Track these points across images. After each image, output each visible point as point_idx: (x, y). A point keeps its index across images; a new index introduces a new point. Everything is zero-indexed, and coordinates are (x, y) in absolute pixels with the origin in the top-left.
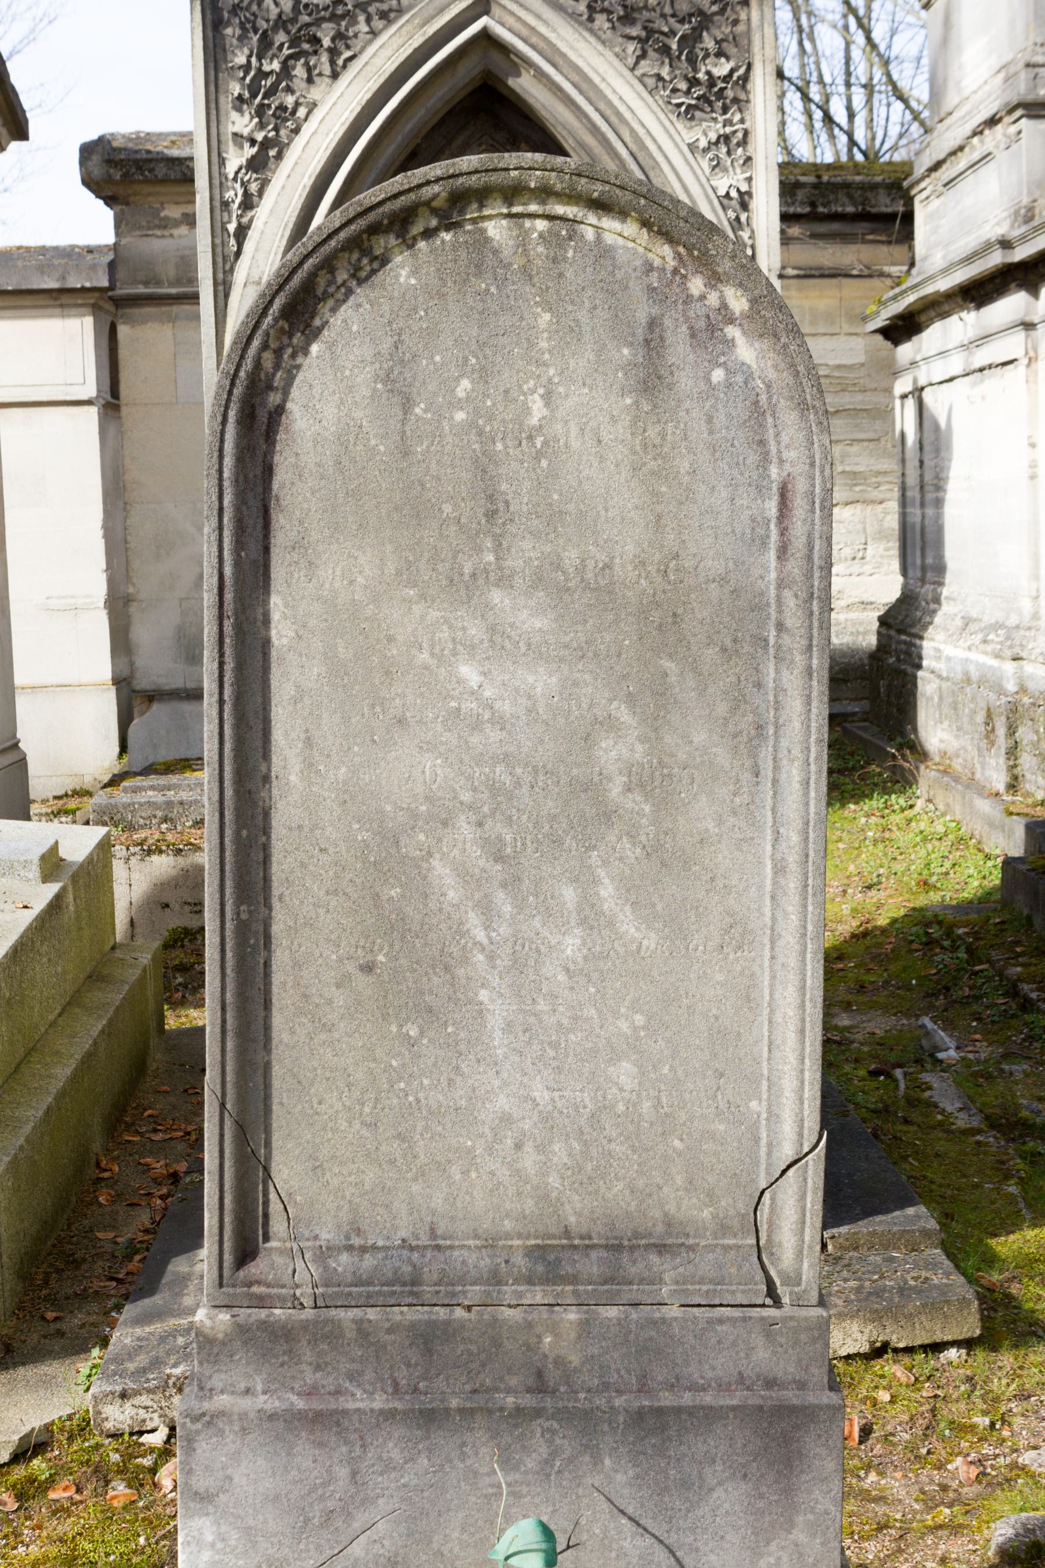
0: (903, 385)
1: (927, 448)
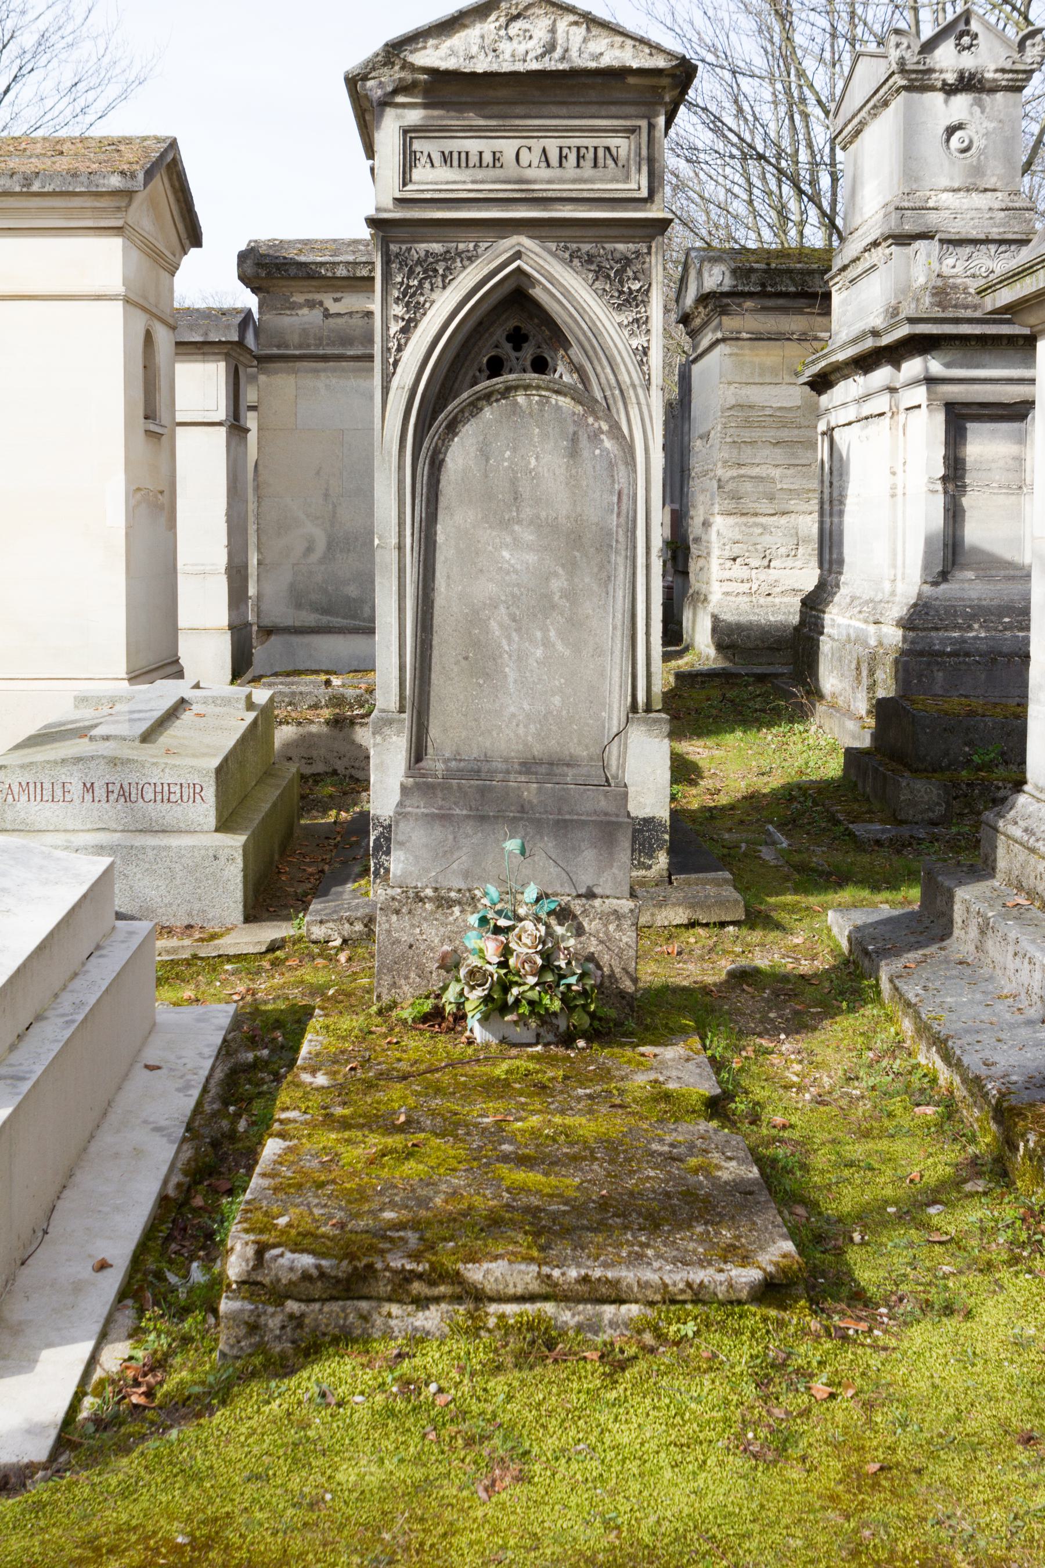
0: (822, 427)
1: (835, 473)
